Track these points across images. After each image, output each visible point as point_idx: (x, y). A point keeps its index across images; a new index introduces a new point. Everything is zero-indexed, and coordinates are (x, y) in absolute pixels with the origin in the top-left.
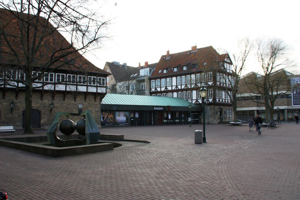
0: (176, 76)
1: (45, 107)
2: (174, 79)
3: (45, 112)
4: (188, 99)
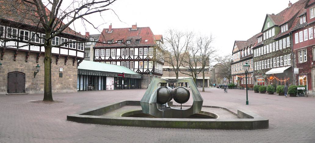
0: (121, 48)
1: (30, 70)
2: (119, 50)
3: (29, 75)
4: (130, 68)
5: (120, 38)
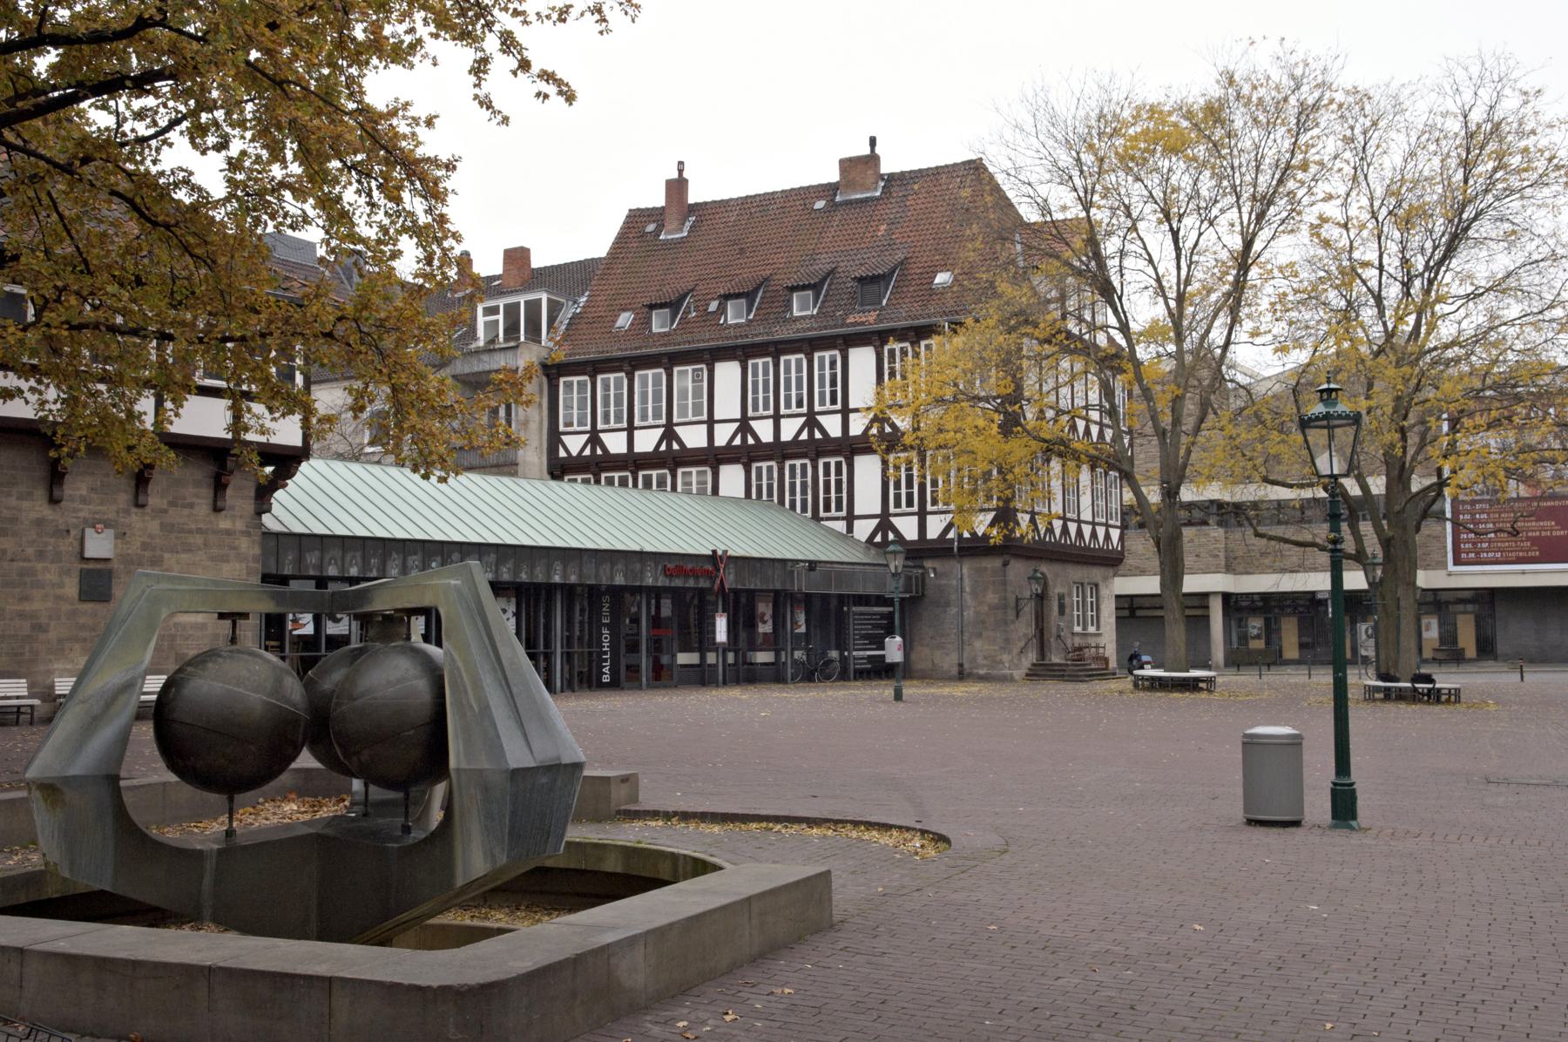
0: (742, 353)
2: (728, 374)
4: (822, 514)
5: (746, 275)
